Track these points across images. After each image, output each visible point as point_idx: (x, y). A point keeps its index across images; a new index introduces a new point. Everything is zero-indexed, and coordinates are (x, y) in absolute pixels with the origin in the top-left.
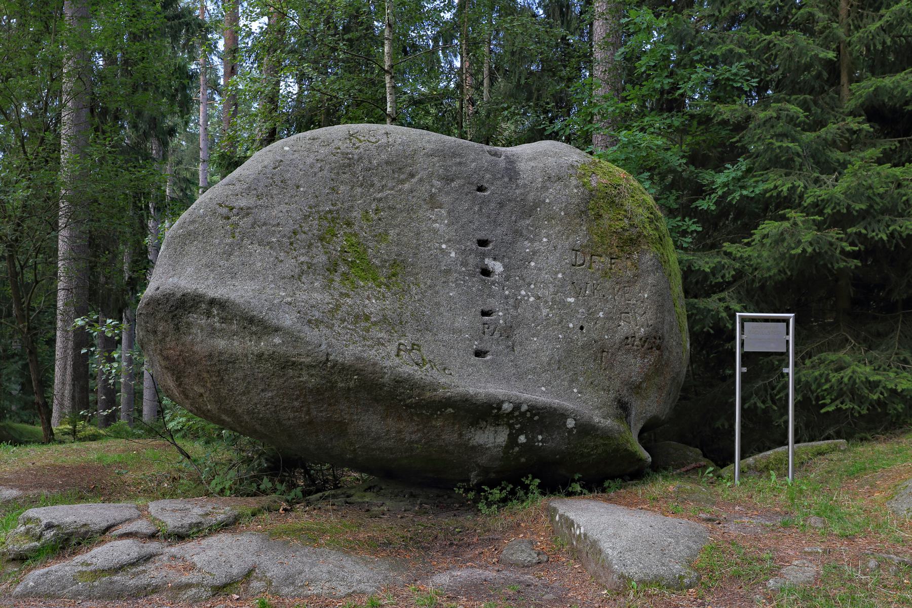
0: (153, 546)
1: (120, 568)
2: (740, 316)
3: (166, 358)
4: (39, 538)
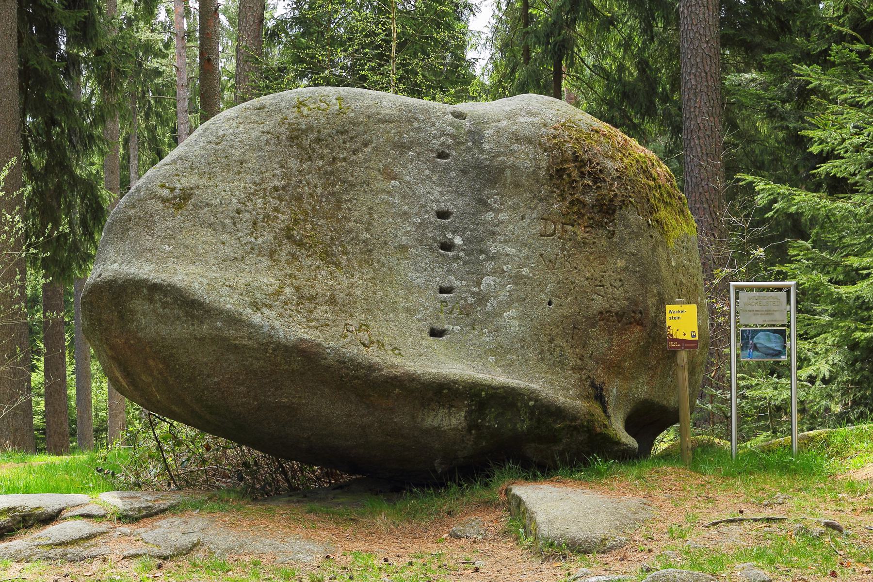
0: (104, 526)
1: (75, 542)
2: (734, 285)
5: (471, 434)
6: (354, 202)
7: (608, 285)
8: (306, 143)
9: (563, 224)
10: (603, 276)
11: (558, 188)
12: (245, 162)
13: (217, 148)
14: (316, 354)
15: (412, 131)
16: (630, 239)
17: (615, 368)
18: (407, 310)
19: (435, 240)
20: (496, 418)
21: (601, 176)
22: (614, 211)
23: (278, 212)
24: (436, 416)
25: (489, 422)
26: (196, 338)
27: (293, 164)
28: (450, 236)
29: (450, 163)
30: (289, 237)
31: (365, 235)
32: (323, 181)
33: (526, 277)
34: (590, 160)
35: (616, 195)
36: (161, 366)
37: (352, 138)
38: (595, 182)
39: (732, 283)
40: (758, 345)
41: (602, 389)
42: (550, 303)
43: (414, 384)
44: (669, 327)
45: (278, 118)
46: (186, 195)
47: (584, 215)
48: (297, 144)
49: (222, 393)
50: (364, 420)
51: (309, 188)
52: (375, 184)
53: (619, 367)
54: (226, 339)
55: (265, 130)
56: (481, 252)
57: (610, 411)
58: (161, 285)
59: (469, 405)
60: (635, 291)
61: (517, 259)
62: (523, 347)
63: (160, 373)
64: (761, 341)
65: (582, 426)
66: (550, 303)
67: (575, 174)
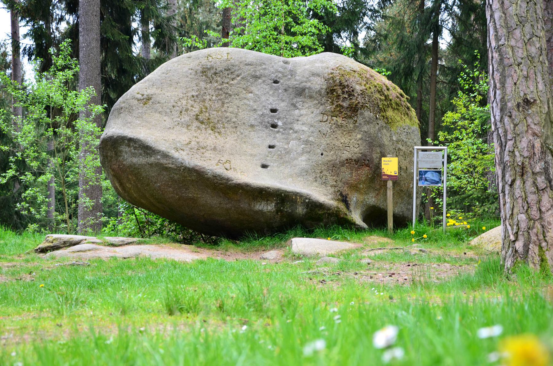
3: (113, 170)
4: (52, 242)
5: (278, 214)
6: (231, 103)
7: (352, 146)
8: (209, 75)
9: (332, 116)
10: (349, 142)
11: (330, 99)
12: (179, 82)
13: (166, 76)
14: (203, 172)
15: (262, 70)
16: (364, 124)
17: (354, 187)
18: (251, 155)
19: (268, 123)
20: (290, 207)
21: (352, 93)
22: (358, 111)
23: (193, 107)
24: (260, 205)
25: (286, 209)
26: (148, 164)
27: (203, 85)
28: (276, 121)
29: (279, 86)
30: (197, 119)
31: (234, 120)
32: (216, 93)
33: (311, 141)
34: (348, 85)
35: (359, 102)
36: (134, 178)
37: (232, 73)
38: (349, 96)
39: (415, 147)
40: (427, 178)
41: (346, 197)
42: (322, 154)
43: (248, 188)
45: (197, 62)
46: (149, 99)
47: (342, 112)
48: (205, 75)
49: (162, 191)
50: (227, 206)
51: (209, 97)
52: (242, 95)
53: (357, 187)
54: (161, 164)
55: (190, 68)
56: (291, 129)
57: (352, 208)
58: (133, 138)
59: (276, 200)
60: (365, 150)
61: (307, 133)
62: (307, 174)
63: (135, 182)
64: (429, 176)
65: (333, 213)
66: (322, 154)
67: (340, 92)
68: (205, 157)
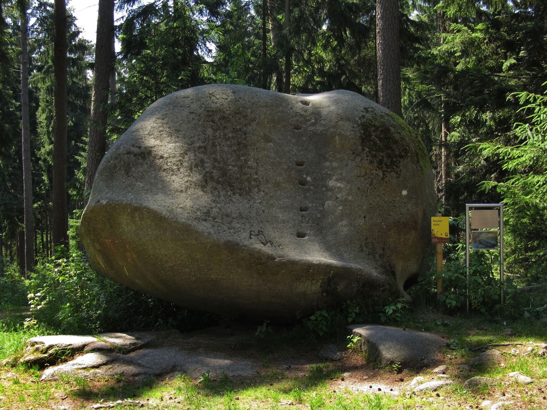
36: (134, 256)
40: (482, 241)
44: (433, 230)
56: (323, 186)
68: (234, 228)
